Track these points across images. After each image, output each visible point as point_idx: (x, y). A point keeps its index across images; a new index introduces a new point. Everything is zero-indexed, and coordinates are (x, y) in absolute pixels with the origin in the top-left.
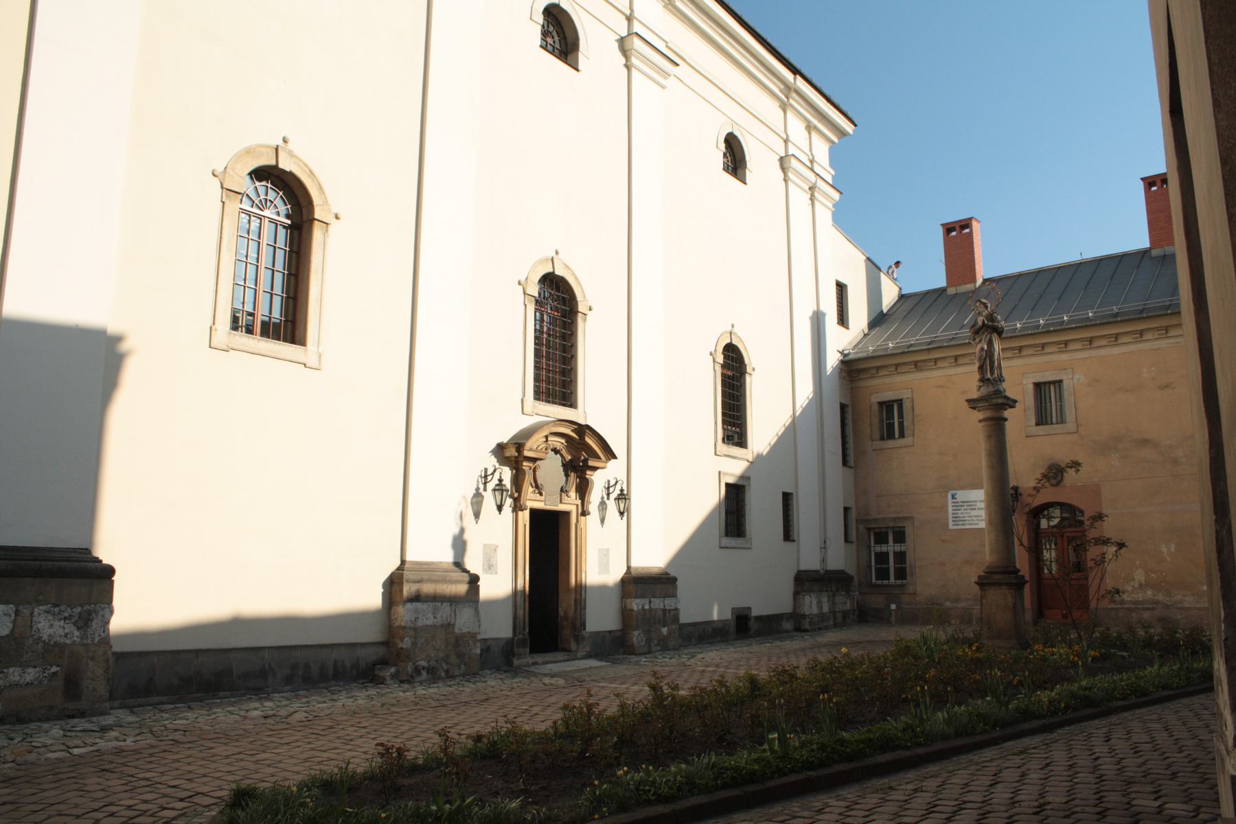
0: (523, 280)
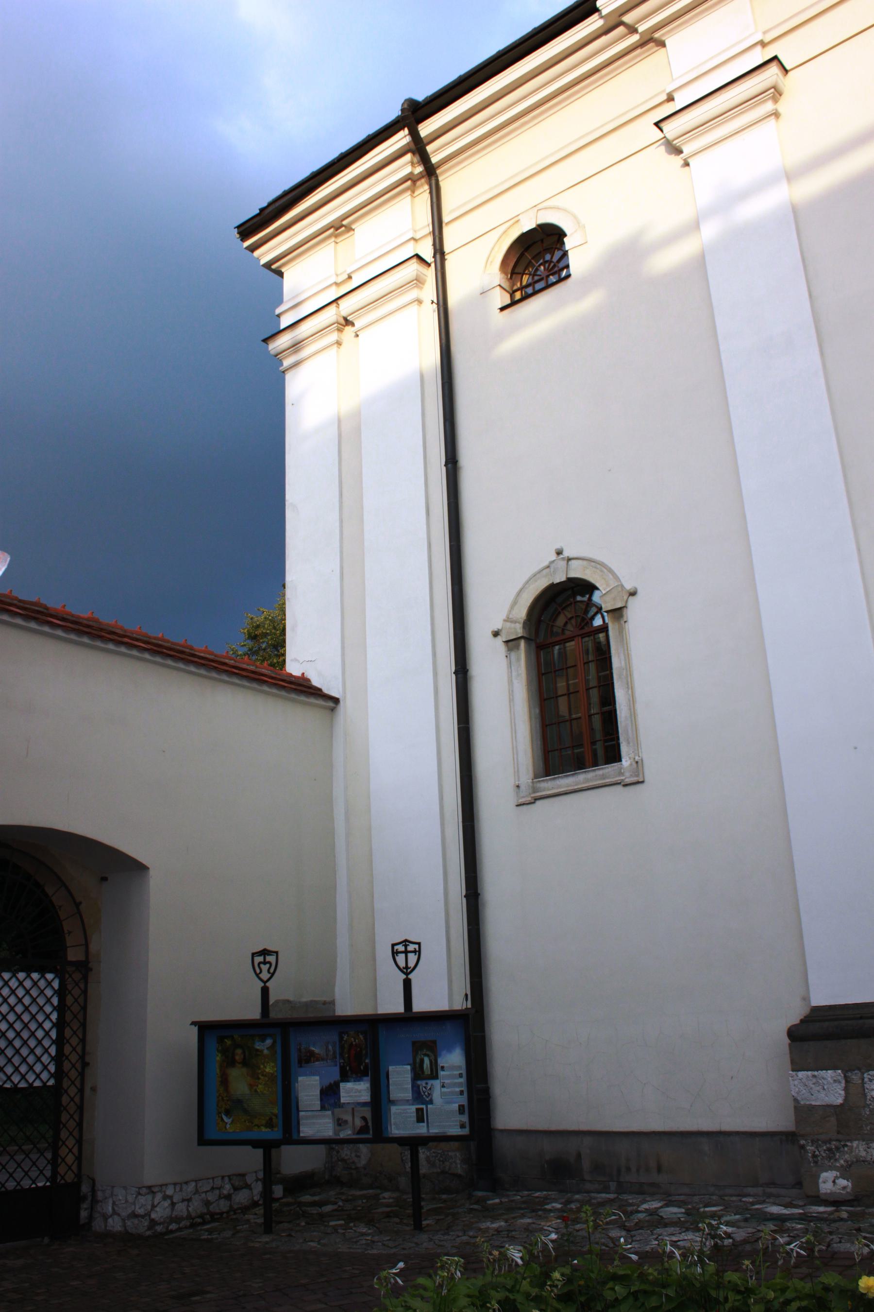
0: (566, 554)
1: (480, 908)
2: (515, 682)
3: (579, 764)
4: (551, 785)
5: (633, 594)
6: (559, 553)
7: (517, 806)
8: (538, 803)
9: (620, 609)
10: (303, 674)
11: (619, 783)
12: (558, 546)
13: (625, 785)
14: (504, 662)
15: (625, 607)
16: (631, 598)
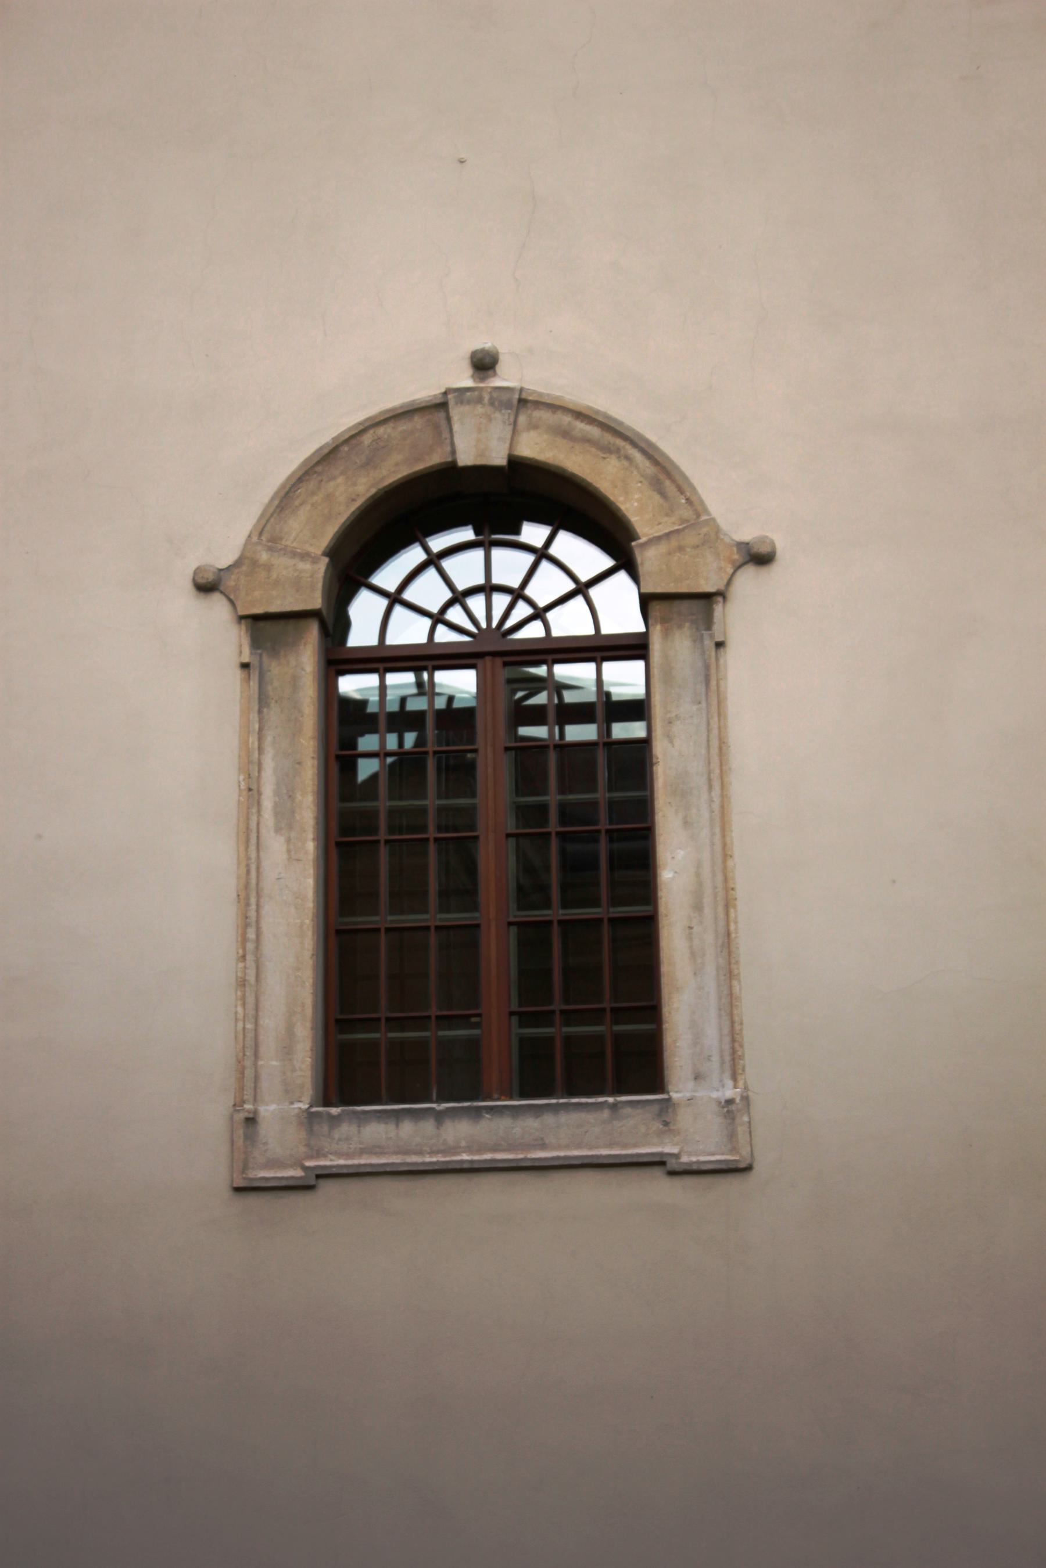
0: (506, 378)
1: (320, 1032)
2: (275, 847)
3: (452, 1077)
4: (377, 1134)
5: (760, 558)
6: (484, 364)
7: (238, 1190)
8: (328, 1188)
9: (707, 598)
10: (397, 1126)
11: (662, 1163)
12: (482, 342)
13: (672, 1173)
14: (229, 688)
15: (722, 594)
16: (750, 570)
